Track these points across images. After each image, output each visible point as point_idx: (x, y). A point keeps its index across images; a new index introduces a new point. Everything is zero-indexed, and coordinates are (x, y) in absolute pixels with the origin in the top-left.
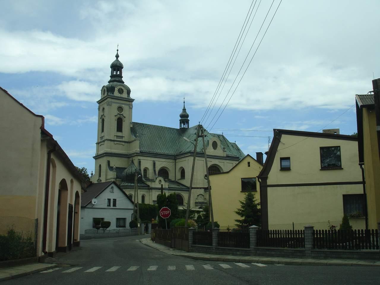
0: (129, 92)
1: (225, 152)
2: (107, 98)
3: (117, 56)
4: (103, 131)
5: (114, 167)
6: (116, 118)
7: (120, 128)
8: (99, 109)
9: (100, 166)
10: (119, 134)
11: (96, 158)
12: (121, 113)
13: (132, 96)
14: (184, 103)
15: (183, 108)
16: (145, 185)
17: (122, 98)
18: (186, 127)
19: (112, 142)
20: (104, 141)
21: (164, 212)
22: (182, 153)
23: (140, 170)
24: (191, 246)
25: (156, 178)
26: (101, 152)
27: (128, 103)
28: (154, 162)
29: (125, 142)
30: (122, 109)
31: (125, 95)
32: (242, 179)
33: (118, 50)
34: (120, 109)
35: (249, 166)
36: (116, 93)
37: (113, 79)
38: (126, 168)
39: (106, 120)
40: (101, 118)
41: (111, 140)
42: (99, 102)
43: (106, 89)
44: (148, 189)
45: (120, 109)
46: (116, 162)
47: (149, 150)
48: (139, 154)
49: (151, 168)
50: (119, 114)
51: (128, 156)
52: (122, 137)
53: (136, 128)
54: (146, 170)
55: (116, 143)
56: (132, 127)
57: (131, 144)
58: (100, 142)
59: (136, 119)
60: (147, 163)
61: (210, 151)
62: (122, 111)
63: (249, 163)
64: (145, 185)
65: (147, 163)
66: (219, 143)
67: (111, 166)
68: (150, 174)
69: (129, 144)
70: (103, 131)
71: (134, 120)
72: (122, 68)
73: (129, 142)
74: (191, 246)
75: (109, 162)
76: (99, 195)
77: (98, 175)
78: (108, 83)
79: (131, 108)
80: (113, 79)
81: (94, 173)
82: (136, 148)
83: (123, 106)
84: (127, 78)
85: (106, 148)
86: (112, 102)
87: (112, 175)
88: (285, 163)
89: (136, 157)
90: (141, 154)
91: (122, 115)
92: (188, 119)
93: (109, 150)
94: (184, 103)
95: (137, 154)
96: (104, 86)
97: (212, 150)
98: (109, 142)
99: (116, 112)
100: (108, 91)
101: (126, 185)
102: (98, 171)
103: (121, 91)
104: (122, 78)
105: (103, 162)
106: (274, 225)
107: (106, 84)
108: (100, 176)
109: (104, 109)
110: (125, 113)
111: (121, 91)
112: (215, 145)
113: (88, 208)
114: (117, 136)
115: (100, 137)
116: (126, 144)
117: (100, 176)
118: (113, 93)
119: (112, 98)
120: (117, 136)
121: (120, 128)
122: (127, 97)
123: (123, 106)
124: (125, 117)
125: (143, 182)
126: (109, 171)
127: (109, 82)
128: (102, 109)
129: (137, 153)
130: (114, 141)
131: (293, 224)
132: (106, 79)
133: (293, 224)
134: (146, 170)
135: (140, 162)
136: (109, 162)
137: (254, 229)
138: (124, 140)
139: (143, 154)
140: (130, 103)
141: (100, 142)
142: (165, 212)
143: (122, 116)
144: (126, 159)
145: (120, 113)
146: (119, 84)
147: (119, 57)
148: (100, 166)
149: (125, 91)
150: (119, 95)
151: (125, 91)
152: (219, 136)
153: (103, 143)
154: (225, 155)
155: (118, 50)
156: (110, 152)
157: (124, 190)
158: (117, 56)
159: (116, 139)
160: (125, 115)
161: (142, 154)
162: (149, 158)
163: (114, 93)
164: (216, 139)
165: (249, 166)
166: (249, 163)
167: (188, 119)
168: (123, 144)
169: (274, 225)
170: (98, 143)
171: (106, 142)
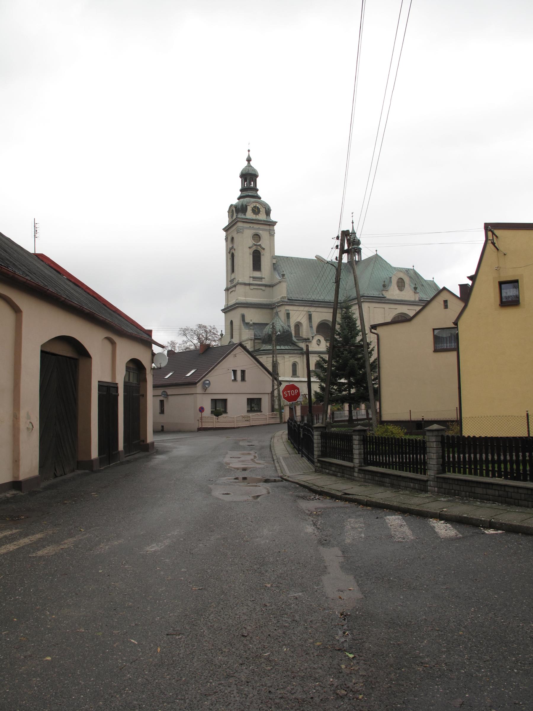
0: (268, 212)
1: (418, 295)
2: (236, 223)
3: (249, 160)
4: (233, 271)
5: (251, 323)
6: (252, 251)
7: (257, 265)
8: (226, 239)
9: (232, 322)
10: (257, 274)
11: (226, 311)
12: (258, 244)
13: (273, 217)
14: (353, 223)
15: (246, 157)
16: (296, 348)
17: (259, 220)
18: (357, 260)
19: (248, 287)
20: (235, 286)
21: (289, 391)
22: (351, 298)
23: (289, 326)
24: (318, 460)
25: (313, 337)
26: (231, 303)
27: (267, 227)
28: (310, 313)
29: (266, 286)
30: (260, 238)
31: (262, 217)
32: (436, 332)
33: (249, 151)
34: (257, 237)
35: (446, 307)
36: (249, 214)
37: (245, 193)
38: (267, 324)
39: (236, 255)
40: (229, 253)
41: (245, 284)
42: (226, 229)
43: (234, 209)
44: (300, 354)
45: (257, 237)
46: (253, 316)
47: (301, 297)
48: (287, 302)
49: (304, 322)
50: (255, 245)
51: (270, 307)
52: (262, 278)
53: (278, 263)
54: (298, 326)
55: (252, 287)
56: (275, 262)
57: (274, 288)
58: (230, 288)
59: (279, 251)
60: (298, 315)
61: (393, 293)
62: (260, 240)
63: (446, 302)
64: (296, 348)
65: (298, 315)
66: (407, 280)
67: (246, 321)
68: (305, 332)
69: (271, 288)
70: (233, 271)
71: (278, 253)
72: (256, 176)
73: (271, 286)
74: (318, 460)
75: (243, 316)
76: (216, 366)
77: (229, 336)
78: (238, 201)
79: (272, 234)
80: (245, 193)
81: (224, 333)
82: (281, 292)
83: (261, 232)
84: (265, 190)
85: (242, 295)
86: (243, 228)
87: (246, 335)
88: (509, 292)
89: (283, 307)
90: (290, 302)
91: (260, 245)
92: (360, 246)
93: (242, 299)
94: (353, 223)
95: (281, 303)
96: (231, 206)
97: (397, 291)
98: (243, 286)
99: (250, 242)
100: (237, 211)
101: (268, 349)
102: (229, 331)
103: (256, 211)
104: (258, 192)
105: (236, 316)
106: (486, 416)
107: (235, 201)
108: (232, 337)
109: (233, 238)
110: (264, 243)
111: (256, 211)
112: (401, 284)
113: (273, 381)
114: (254, 278)
115: (229, 280)
116: (268, 289)
117: (232, 337)
118: (245, 215)
119: (244, 222)
120: (254, 278)
121: (257, 265)
122: (265, 220)
123: (261, 232)
124: (264, 249)
125: (294, 344)
126: (243, 327)
127: (239, 199)
128: (230, 240)
129: (283, 301)
130: (249, 284)
131: (527, 414)
132: (232, 193)
133: (527, 414)
134: (298, 326)
135: (288, 315)
136: (243, 316)
137: (435, 433)
138: (263, 282)
139: (292, 302)
140: (271, 228)
141: (230, 288)
142: (290, 392)
143: (259, 247)
144: (268, 311)
145: (257, 242)
146: (253, 200)
147: (251, 160)
148: (232, 322)
149: (263, 210)
150: (253, 217)
151: (263, 210)
152: (407, 271)
153: (233, 289)
154: (417, 299)
155: (249, 151)
156: (244, 301)
157: (257, 357)
158: (249, 160)
159: (252, 282)
160: (263, 246)
161: (291, 302)
162: (302, 308)
163: (247, 214)
164: (402, 275)
165: (446, 307)
166: (446, 302)
167: (360, 246)
168: (263, 288)
169: (486, 416)
170: (227, 290)
171: (238, 287)
